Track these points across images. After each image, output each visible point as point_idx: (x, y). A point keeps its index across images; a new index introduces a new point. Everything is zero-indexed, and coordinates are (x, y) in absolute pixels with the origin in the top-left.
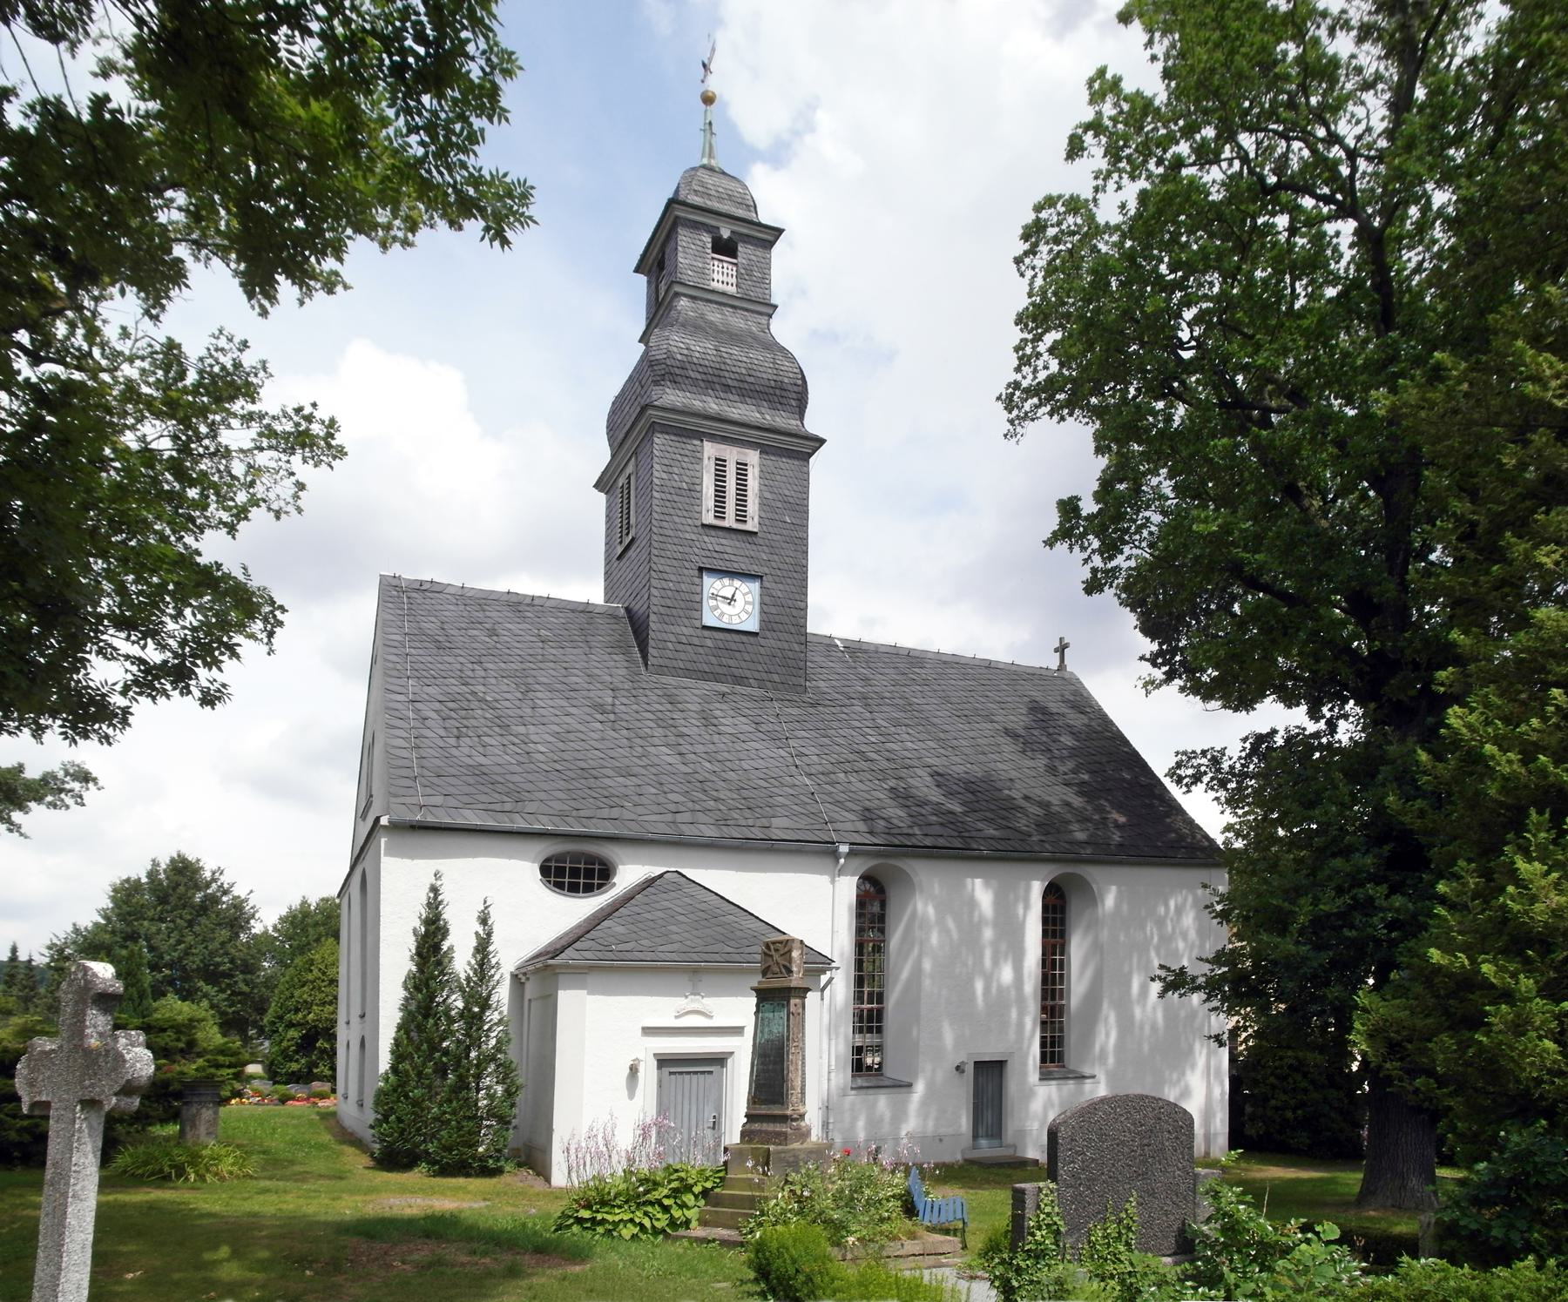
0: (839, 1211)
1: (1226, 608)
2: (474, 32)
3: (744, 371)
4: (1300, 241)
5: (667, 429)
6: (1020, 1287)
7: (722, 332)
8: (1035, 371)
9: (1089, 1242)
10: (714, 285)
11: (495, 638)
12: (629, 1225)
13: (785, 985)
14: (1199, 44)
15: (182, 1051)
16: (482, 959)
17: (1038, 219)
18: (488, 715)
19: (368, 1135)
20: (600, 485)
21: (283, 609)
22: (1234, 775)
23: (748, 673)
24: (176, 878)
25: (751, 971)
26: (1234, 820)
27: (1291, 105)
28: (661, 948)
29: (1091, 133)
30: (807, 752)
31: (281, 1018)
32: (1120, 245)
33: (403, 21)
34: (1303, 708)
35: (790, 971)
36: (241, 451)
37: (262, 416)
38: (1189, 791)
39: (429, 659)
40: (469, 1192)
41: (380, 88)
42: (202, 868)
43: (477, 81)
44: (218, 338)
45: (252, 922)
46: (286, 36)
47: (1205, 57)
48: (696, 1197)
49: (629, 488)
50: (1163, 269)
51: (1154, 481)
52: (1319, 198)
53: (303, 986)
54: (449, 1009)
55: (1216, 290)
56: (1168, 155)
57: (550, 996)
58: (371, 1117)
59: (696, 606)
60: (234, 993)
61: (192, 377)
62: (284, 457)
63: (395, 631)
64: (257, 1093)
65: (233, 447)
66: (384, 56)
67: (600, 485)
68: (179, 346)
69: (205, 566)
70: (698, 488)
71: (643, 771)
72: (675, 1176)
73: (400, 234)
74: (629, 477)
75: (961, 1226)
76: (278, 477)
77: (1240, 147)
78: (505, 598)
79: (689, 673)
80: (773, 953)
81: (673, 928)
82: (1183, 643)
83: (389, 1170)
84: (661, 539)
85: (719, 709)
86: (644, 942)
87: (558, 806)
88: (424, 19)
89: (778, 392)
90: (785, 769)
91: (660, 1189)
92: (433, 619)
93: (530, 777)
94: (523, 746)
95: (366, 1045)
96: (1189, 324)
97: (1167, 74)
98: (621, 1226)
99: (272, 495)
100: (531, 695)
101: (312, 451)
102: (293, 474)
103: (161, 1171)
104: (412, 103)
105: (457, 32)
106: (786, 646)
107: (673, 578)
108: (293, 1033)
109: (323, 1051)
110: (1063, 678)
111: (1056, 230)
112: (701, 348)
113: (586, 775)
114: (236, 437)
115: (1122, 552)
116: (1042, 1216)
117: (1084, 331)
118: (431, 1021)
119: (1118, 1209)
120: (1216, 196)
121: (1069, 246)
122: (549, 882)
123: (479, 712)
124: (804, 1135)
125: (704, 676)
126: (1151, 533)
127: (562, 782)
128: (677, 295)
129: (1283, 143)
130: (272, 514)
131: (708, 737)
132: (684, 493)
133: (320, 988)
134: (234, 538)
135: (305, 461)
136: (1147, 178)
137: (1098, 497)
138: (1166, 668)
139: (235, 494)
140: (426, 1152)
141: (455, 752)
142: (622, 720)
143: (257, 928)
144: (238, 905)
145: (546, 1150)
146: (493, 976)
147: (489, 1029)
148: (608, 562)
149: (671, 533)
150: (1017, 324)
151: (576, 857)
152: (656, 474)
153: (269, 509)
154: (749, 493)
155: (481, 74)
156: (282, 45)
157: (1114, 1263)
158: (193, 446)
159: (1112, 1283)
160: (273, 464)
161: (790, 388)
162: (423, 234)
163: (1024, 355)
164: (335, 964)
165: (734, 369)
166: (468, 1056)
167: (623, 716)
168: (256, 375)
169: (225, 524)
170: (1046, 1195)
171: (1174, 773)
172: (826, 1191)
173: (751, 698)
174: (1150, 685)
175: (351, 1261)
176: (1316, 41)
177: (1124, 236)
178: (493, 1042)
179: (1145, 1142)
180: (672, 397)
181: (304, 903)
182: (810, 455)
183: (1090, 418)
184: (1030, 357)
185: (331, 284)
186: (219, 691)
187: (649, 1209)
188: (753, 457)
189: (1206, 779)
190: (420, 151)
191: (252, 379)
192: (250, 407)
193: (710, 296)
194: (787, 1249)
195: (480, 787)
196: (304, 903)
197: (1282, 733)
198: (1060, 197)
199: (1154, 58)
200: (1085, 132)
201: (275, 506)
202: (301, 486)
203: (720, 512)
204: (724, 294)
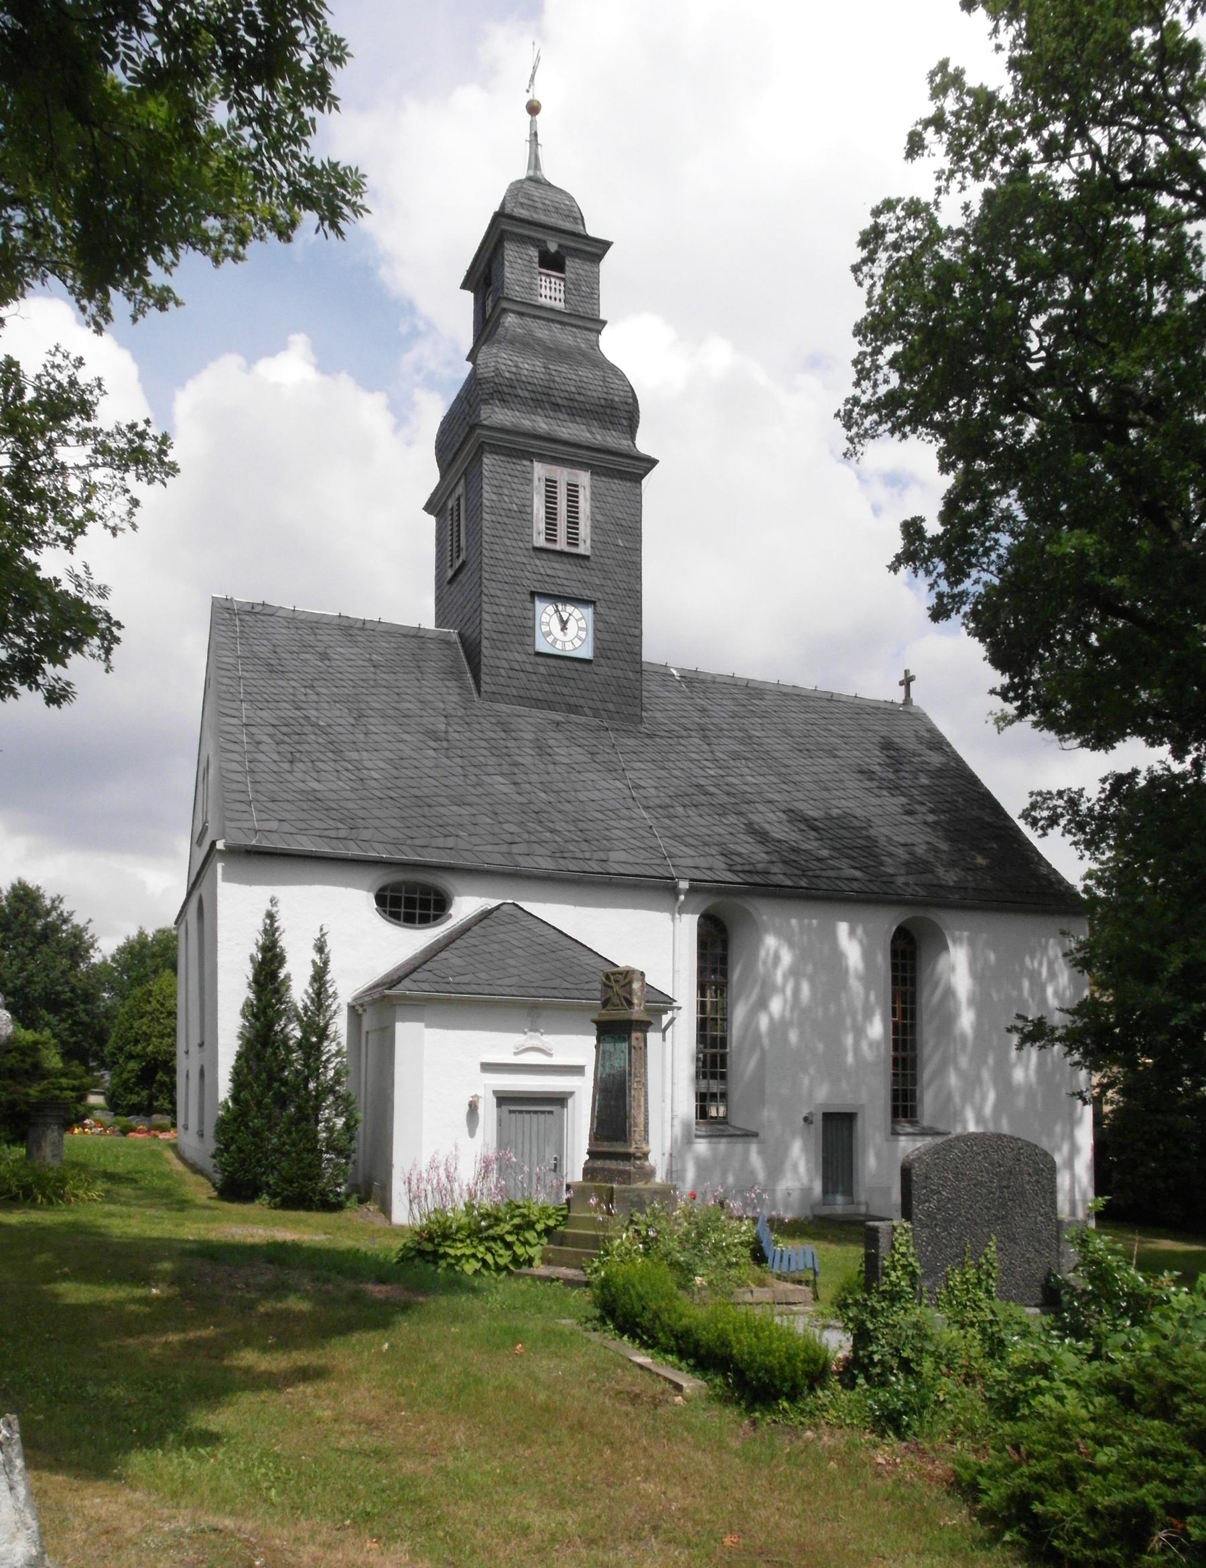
0: (686, 1253)
1: (1083, 639)
2: (305, 22)
3: (573, 389)
4: (1158, 243)
5: (497, 450)
6: (875, 1330)
7: (550, 349)
8: (875, 386)
9: (947, 1286)
10: (543, 301)
11: (327, 662)
12: (472, 1261)
13: (626, 1017)
14: (1048, 32)
15: (27, 1072)
16: (320, 988)
17: (876, 225)
18: (321, 741)
19: (209, 1164)
20: (429, 507)
21: (119, 625)
22: (1093, 818)
23: (582, 702)
24: (18, 905)
25: (590, 1008)
26: (1095, 866)
27: (1147, 95)
28: (499, 982)
29: (931, 129)
30: (643, 784)
31: (120, 1049)
32: (963, 250)
33: (235, 14)
34: (1167, 747)
35: (630, 1004)
36: (77, 467)
37: (96, 433)
38: (1045, 834)
39: (262, 682)
40: (309, 1226)
41: (214, 81)
42: (43, 896)
43: (307, 69)
44: (54, 355)
45: (91, 951)
46: (123, 30)
47: (1054, 45)
48: (539, 1234)
49: (459, 510)
50: (1011, 274)
51: (1004, 503)
52: (1178, 194)
53: (142, 1017)
54: (287, 1038)
55: (1067, 295)
56: (1014, 153)
57: (387, 1027)
58: (211, 1145)
59: (529, 631)
60: (75, 1023)
61: (30, 394)
62: (119, 475)
63: (228, 653)
64: (99, 1123)
65: (69, 464)
66: (217, 47)
67: (429, 507)
68: (17, 364)
69: (44, 580)
70: (529, 510)
71: (476, 800)
72: (517, 1212)
73: (231, 248)
74: (459, 499)
75: (812, 1278)
76: (113, 494)
77: (1091, 141)
78: (336, 621)
79: (522, 700)
80: (613, 984)
81: (510, 961)
82: (1036, 676)
83: (231, 1201)
84: (492, 562)
85: (553, 739)
86: (481, 975)
87: (392, 833)
88: (256, 9)
89: (608, 411)
90: (621, 801)
91: (502, 1225)
92: (265, 642)
93: (363, 804)
94: (356, 772)
95: (206, 1074)
96: (1038, 334)
97: (1014, 64)
98: (463, 1261)
99: (108, 512)
100: (363, 720)
101: (145, 468)
102: (127, 491)
103: (9, 1191)
104: (244, 95)
105: (288, 20)
106: (620, 673)
107: (504, 602)
108: (133, 1065)
109: (162, 1084)
110: (910, 713)
111: (896, 235)
112: (530, 366)
113: (421, 803)
114: (71, 454)
115: (968, 576)
116: (897, 1256)
117: (926, 341)
118: (270, 1050)
119: (976, 1254)
120: (1067, 195)
121: (910, 252)
122: (385, 911)
123: (313, 737)
124: (649, 1174)
125: (537, 703)
126: (1000, 556)
127: (396, 810)
128: (505, 311)
129: (1139, 139)
130: (109, 531)
131: (542, 766)
132: (514, 515)
133: (158, 1020)
134: (71, 552)
135: (139, 478)
136: (992, 179)
137: (944, 518)
138: (1018, 703)
139: (72, 508)
140: (268, 1185)
141: (289, 777)
142: (456, 748)
143: (96, 958)
144: (78, 933)
145: (386, 1187)
146: (330, 1006)
147: (328, 1060)
148: (439, 587)
149: (501, 556)
150: (855, 335)
151: (413, 887)
152: (485, 495)
153: (106, 526)
154: (581, 515)
155: (311, 62)
156: (120, 40)
157: (974, 1310)
158: (31, 463)
159: (972, 1331)
160: (108, 481)
161: (620, 406)
162: (253, 246)
163: (863, 369)
164: (173, 995)
165: (563, 388)
166: (306, 1087)
167: (457, 743)
168: (91, 392)
169: (63, 539)
170: (901, 1234)
171: (1029, 815)
172: (672, 1233)
173: (586, 728)
174: (1004, 721)
175: (196, 1282)
176: (1174, 26)
177: (967, 241)
178: (331, 1073)
179: (1004, 1183)
180: (498, 415)
181: (141, 934)
182: (643, 476)
183: (934, 436)
184: (869, 371)
185: (163, 299)
186: (64, 689)
187: (492, 1244)
188: (584, 478)
189: (1063, 822)
190: (253, 144)
191: (87, 397)
192: (86, 424)
193: (537, 313)
194: (633, 1286)
195: (315, 813)
196: (141, 934)
197: (1144, 773)
198: (899, 200)
199: (999, 48)
200: (925, 128)
201: (111, 523)
202: (135, 503)
203: (551, 536)
204: (552, 310)
